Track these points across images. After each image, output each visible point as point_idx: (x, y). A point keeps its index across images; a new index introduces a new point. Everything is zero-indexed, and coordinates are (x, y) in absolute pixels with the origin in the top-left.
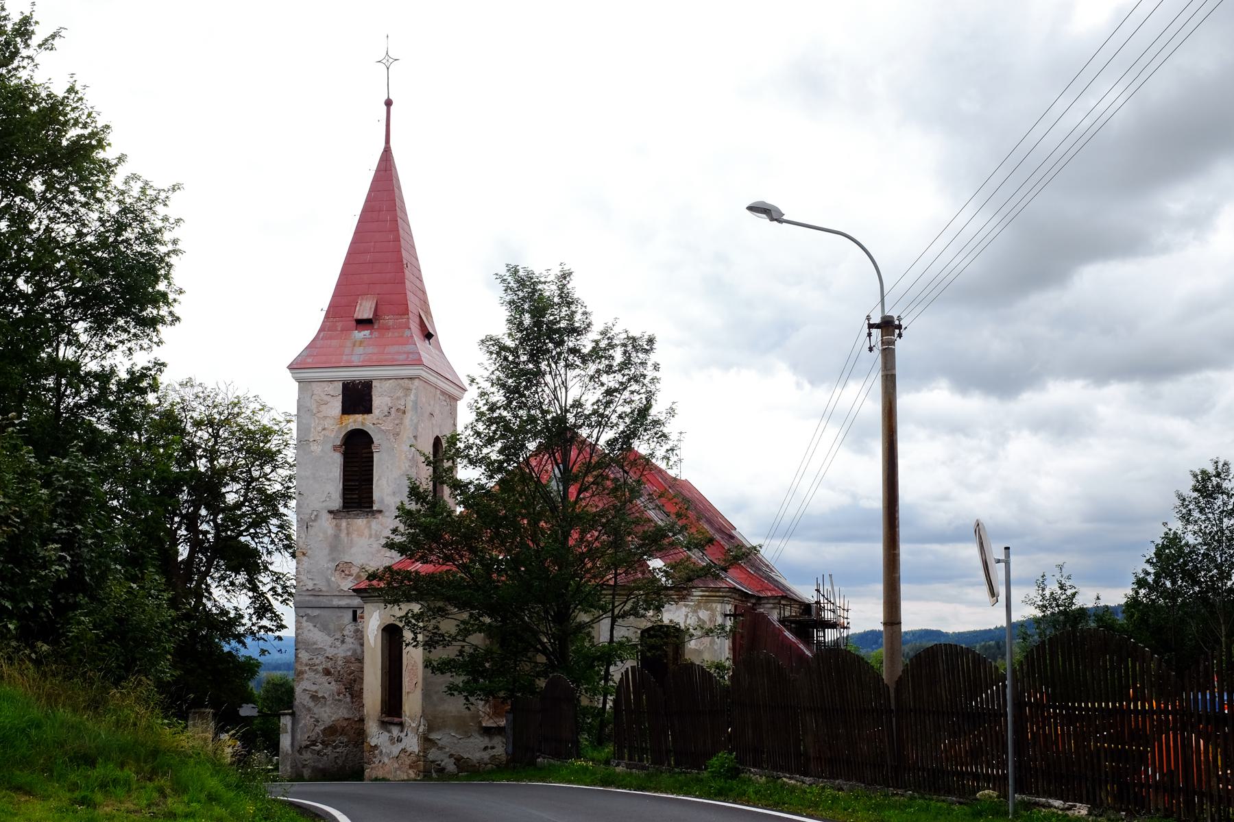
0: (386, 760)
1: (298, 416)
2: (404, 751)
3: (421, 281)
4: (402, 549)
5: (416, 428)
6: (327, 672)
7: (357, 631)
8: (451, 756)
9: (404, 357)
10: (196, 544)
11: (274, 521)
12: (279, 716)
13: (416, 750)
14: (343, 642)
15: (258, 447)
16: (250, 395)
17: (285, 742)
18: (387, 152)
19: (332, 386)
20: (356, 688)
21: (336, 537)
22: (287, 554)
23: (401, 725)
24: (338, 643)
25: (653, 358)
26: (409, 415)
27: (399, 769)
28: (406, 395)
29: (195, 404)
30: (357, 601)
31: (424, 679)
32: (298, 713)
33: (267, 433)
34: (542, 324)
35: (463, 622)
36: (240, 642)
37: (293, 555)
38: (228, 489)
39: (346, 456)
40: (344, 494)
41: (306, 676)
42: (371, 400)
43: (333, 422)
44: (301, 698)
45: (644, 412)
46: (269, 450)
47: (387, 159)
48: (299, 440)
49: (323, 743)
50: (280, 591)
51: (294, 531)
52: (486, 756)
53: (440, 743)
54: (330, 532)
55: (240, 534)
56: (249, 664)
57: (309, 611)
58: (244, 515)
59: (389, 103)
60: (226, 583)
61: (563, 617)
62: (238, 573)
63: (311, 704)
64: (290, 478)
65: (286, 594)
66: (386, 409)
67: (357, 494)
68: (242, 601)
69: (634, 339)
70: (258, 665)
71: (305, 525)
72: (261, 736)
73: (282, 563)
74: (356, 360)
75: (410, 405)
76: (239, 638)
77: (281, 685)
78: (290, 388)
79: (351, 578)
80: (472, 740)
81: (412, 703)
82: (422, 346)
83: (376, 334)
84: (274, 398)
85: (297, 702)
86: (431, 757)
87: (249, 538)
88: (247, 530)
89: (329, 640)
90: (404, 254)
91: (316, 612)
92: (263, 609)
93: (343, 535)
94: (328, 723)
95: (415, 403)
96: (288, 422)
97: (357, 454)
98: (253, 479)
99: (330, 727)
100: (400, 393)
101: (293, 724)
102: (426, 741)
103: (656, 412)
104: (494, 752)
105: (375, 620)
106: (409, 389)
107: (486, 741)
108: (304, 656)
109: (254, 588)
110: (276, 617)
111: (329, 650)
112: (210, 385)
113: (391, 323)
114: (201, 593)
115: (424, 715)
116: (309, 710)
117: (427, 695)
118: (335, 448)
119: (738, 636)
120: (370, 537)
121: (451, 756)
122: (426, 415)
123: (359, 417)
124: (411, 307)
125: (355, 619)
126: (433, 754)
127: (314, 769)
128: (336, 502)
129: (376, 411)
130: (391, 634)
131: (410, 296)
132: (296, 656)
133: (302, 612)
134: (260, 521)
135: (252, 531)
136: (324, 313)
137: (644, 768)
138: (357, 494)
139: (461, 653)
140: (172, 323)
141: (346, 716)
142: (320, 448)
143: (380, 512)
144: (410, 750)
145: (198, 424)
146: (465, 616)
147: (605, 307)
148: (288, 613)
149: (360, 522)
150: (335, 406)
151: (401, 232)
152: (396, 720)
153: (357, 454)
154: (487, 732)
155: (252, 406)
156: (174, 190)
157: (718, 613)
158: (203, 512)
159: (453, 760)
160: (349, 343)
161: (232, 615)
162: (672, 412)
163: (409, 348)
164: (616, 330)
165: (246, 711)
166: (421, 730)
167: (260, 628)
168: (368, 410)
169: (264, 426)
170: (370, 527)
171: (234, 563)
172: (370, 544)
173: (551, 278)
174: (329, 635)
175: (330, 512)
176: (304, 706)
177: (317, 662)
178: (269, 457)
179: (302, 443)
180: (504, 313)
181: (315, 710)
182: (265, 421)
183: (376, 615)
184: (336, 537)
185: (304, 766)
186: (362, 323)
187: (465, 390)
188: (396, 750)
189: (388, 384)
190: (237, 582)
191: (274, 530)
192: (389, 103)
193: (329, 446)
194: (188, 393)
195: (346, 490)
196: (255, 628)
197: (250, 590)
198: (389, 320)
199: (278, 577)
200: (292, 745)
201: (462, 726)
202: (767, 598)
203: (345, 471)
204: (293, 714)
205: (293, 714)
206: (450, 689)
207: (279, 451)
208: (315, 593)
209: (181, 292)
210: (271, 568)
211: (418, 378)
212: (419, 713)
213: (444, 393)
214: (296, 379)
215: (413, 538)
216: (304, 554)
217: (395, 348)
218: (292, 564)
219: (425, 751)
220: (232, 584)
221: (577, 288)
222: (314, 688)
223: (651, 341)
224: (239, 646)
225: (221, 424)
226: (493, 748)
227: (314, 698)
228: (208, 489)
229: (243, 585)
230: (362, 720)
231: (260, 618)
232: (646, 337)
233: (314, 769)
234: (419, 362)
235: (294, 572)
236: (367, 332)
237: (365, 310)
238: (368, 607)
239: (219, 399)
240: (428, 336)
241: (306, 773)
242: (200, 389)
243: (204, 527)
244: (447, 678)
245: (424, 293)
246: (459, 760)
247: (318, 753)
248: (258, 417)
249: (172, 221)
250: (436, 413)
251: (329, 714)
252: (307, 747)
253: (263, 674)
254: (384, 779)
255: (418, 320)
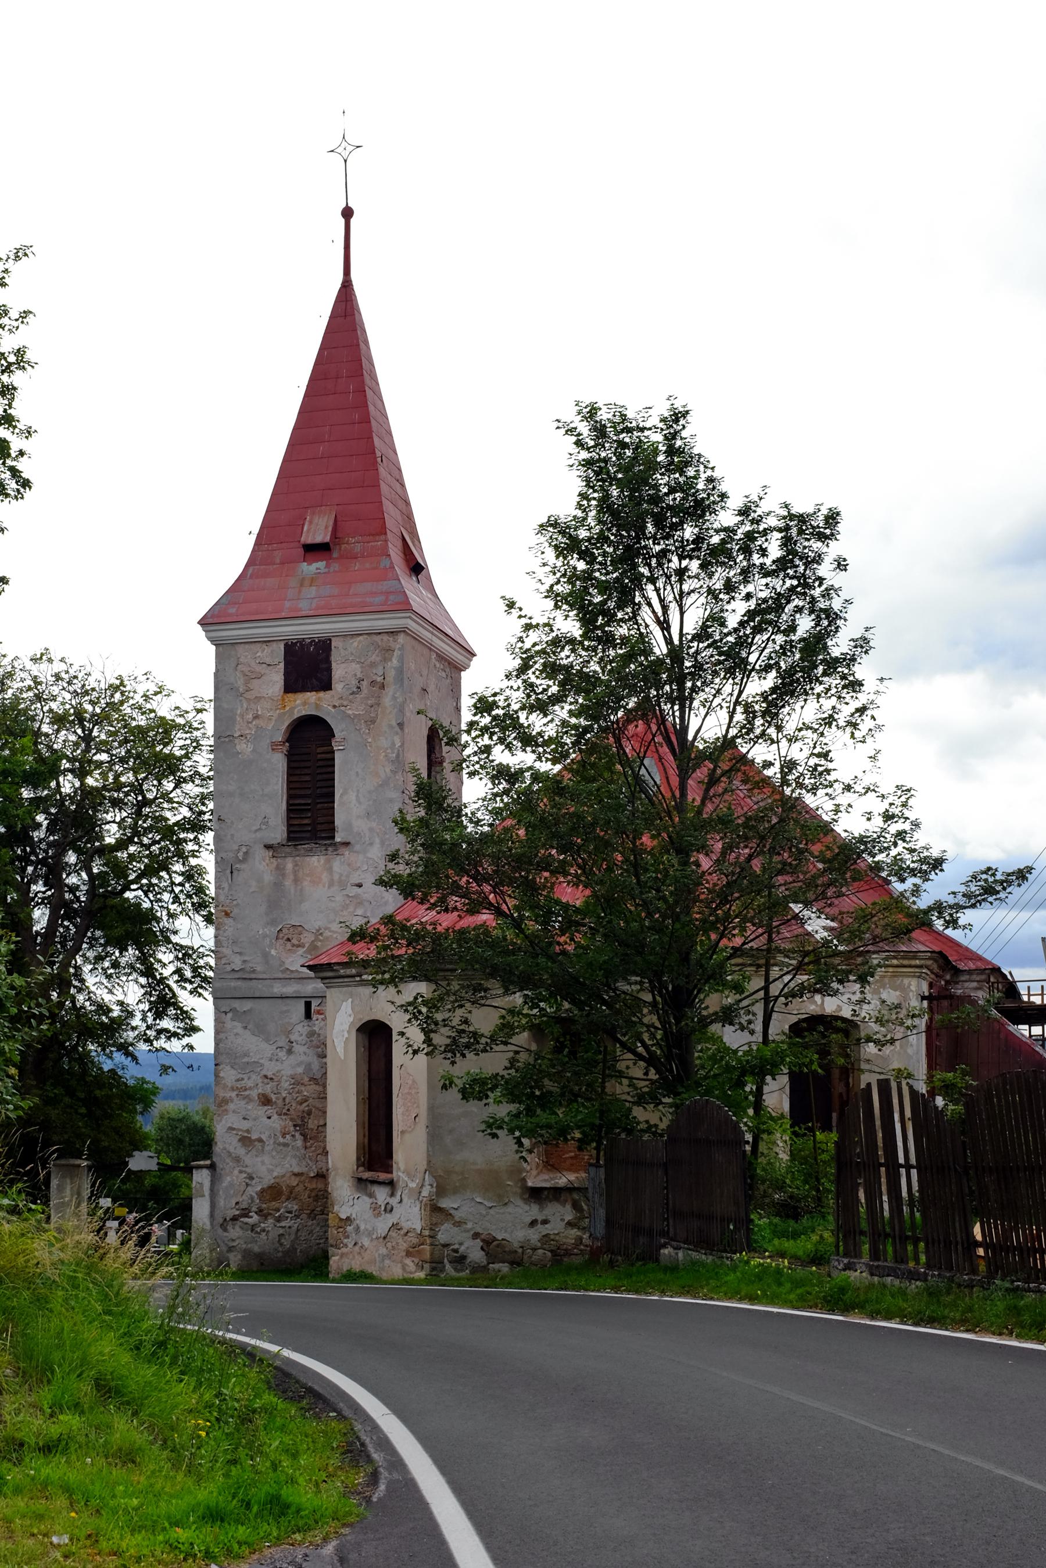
0: (366, 1242)
1: (217, 699)
2: (395, 1226)
3: (403, 485)
4: (408, 888)
5: (401, 711)
6: (265, 1101)
7: (311, 1034)
8: (476, 1235)
9: (382, 598)
10: (59, 907)
11: (178, 867)
12: (189, 1170)
13: (418, 1226)
14: (290, 1052)
15: (152, 749)
16: (139, 673)
17: (201, 1210)
18: (346, 290)
19: (267, 650)
20: (312, 1124)
21: (278, 885)
22: (199, 919)
23: (391, 1184)
24: (282, 1054)
25: (833, 550)
26: (390, 691)
27: (389, 1256)
28: (385, 660)
29: (55, 690)
30: (314, 986)
31: (431, 1109)
32: (220, 1165)
33: (166, 728)
34: (639, 497)
35: (511, 1012)
36: (128, 1054)
37: (208, 919)
38: (109, 817)
39: (290, 757)
40: (289, 818)
41: (231, 1106)
42: (329, 670)
43: (276, 707)
44: (224, 1142)
45: (815, 645)
46: (171, 755)
47: (346, 295)
48: (217, 736)
49: (260, 1212)
50: (188, 974)
51: (210, 880)
52: (533, 1236)
53: (458, 1215)
54: (268, 878)
55: (127, 888)
56: (142, 1089)
57: (236, 1004)
58: (132, 857)
59: (347, 213)
60: (107, 964)
61: (679, 1002)
62: (123, 949)
63: (241, 1151)
64: (203, 798)
65: (199, 981)
66: (354, 682)
67: (310, 816)
68: (132, 992)
69: (802, 519)
70: (155, 1091)
71: (226, 867)
72: (161, 1201)
73: (193, 932)
74: (305, 607)
75: (391, 674)
76: (125, 1048)
77: (180, 1120)
78: (204, 655)
79: (301, 951)
80: (510, 1209)
81: (409, 1147)
82: (408, 584)
83: (335, 566)
84: (179, 674)
85: (218, 1148)
86: (442, 1237)
87: (140, 893)
88: (136, 881)
89: (268, 1049)
90: (377, 441)
91: (247, 1005)
92: (163, 1003)
93: (288, 883)
94: (268, 1180)
95: (400, 671)
96: (199, 711)
97: (309, 749)
98: (146, 803)
99: (270, 1187)
100: (375, 657)
101: (213, 1183)
102: (435, 1211)
103: (839, 646)
104: (547, 1230)
105: (343, 1016)
106: (390, 650)
107: (533, 1211)
108: (229, 1075)
109: (149, 972)
110: (184, 1015)
111: (267, 1063)
112: (77, 660)
113: (358, 548)
114: (65, 981)
115: (430, 1168)
116: (237, 1160)
117: (434, 1136)
118: (274, 746)
119: (934, 1033)
120: (331, 884)
121: (476, 1235)
122: (417, 690)
123: (311, 697)
124: (390, 523)
125: (308, 1015)
126: (446, 1233)
127: (247, 1254)
128: (278, 832)
129: (338, 686)
130: (375, 1037)
131: (387, 506)
132: (217, 1076)
133: (226, 1005)
134: (157, 866)
135: (144, 881)
136: (254, 537)
137: (913, 1276)
138: (310, 816)
139: (513, 1062)
140: (19, 496)
141: (296, 1170)
142: (250, 748)
143: (347, 844)
144: (406, 1225)
145: (60, 720)
146: (518, 999)
147: (749, 467)
148: (202, 1009)
149: (316, 861)
150: (276, 678)
151: (371, 408)
152: (383, 1176)
153: (309, 749)
154: (536, 1195)
155: (141, 689)
156: (17, 258)
157: (912, 990)
158: (72, 858)
159: (478, 1243)
160: (293, 582)
161: (115, 1014)
162: (863, 644)
163: (387, 585)
164: (764, 507)
165: (140, 1162)
166: (425, 1192)
167: (160, 1032)
168: (326, 685)
169: (162, 718)
170: (330, 870)
171: (119, 931)
172: (349, 889)
173: (654, 421)
174: (267, 1040)
175: (268, 847)
176: (229, 1154)
177: (250, 1084)
178: (170, 766)
179: (223, 739)
180: (573, 483)
181: (248, 1160)
182: (164, 709)
183: (346, 1007)
184: (278, 885)
185: (230, 1249)
186: (314, 550)
187: (474, 655)
188: (383, 1225)
189: (355, 643)
190: (123, 961)
191: (179, 879)
192: (347, 213)
193: (265, 743)
194: (45, 671)
195: (293, 811)
196: (151, 1033)
197: (142, 974)
198: (354, 544)
199: (185, 953)
200: (212, 1215)
201: (492, 1184)
202: (970, 972)
203: (289, 782)
204: (212, 1167)
205: (212, 1167)
206: (490, 1126)
207: (187, 756)
208: (246, 975)
209: (29, 433)
210: (175, 939)
211: (404, 631)
212: (423, 1165)
213: (441, 657)
214: (212, 640)
215: (431, 870)
216: (227, 914)
217: (368, 586)
218: (209, 932)
219: (433, 1227)
220: (115, 965)
221: (701, 436)
222: (245, 1125)
223: (832, 518)
224: (128, 1062)
225: (98, 720)
226: (545, 1222)
227: (246, 1141)
228: (78, 822)
229: (132, 967)
230: (322, 1176)
231: (159, 1015)
232: (824, 511)
233: (247, 1254)
234: (405, 606)
235: (211, 944)
236: (321, 564)
237: (318, 531)
238: (333, 995)
239: (92, 683)
240: (417, 568)
241: (235, 1260)
242: (63, 667)
243: (73, 880)
244: (478, 1111)
245: (407, 503)
246: (489, 1244)
247: (253, 1228)
248: (152, 705)
249: (14, 314)
250: (431, 688)
251: (273, 1165)
252: (234, 1219)
253: (162, 1106)
254: (364, 1276)
255: (399, 543)
